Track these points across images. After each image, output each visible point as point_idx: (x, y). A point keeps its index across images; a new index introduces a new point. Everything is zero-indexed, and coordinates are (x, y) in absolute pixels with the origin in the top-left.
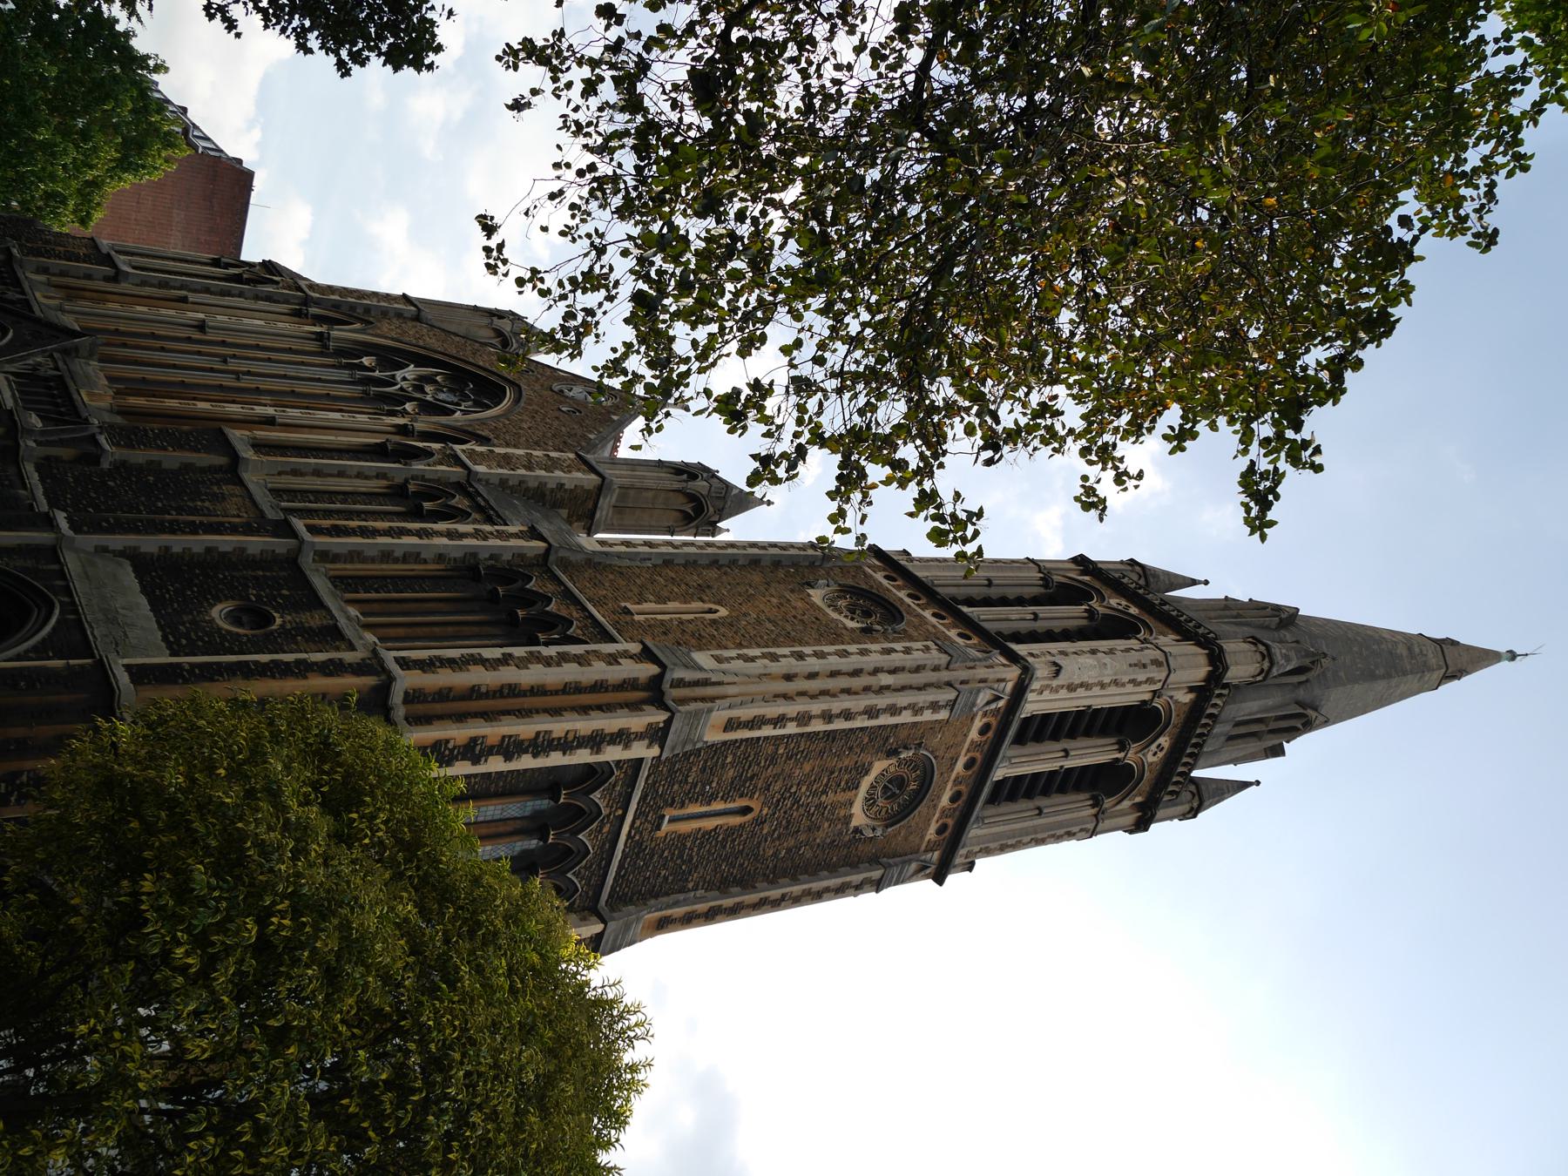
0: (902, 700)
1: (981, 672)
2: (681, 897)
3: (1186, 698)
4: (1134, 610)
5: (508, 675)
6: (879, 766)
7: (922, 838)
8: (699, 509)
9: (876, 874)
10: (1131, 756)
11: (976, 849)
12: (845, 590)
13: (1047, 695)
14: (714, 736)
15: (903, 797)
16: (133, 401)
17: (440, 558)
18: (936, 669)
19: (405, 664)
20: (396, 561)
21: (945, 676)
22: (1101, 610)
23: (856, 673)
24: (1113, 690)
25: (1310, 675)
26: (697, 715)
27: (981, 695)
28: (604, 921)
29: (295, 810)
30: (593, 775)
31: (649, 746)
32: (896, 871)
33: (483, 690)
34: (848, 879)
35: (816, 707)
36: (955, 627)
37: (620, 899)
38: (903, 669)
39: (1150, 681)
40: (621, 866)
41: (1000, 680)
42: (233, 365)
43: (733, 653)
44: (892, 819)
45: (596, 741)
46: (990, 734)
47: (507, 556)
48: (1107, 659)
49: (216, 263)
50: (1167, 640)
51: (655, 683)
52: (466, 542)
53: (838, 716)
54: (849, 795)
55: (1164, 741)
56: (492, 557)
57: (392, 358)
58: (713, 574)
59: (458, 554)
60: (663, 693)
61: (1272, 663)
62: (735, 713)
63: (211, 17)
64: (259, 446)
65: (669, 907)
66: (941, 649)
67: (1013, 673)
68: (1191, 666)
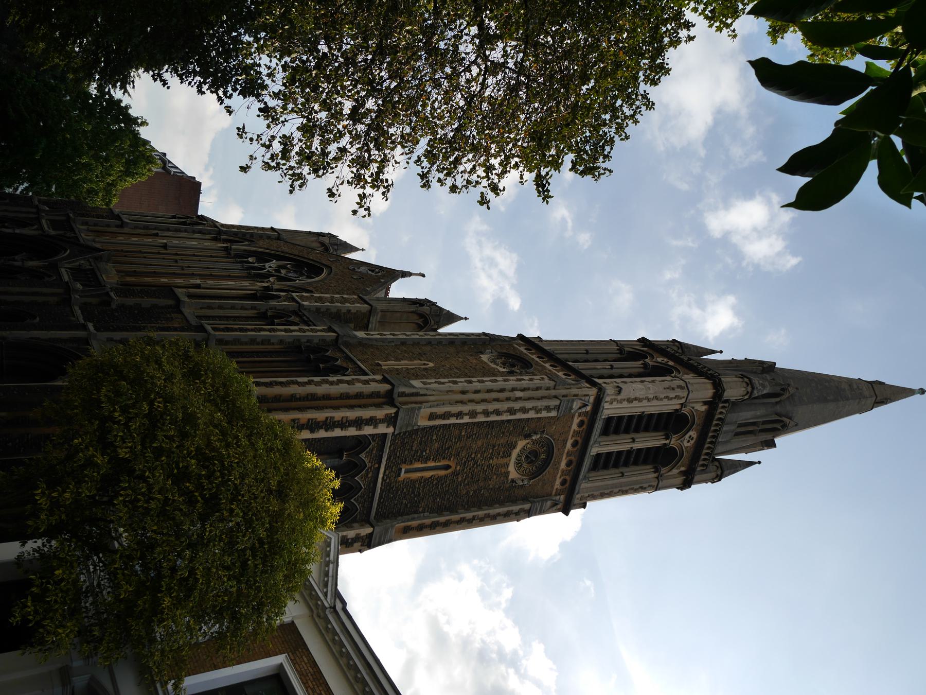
0: (529, 405)
1: (574, 391)
2: (416, 516)
3: (704, 408)
4: (671, 363)
5: (311, 389)
6: (521, 444)
7: (552, 487)
8: (426, 322)
9: (527, 506)
10: (674, 442)
11: (586, 495)
12: (501, 355)
13: (615, 405)
14: (423, 423)
15: (539, 460)
16: (128, 279)
17: (281, 342)
18: (548, 389)
19: (258, 384)
20: (258, 344)
21: (553, 392)
22: (651, 363)
23: (502, 390)
24: (655, 402)
25: (783, 398)
26: (413, 410)
27: (575, 403)
28: (372, 526)
29: (167, 367)
30: (360, 443)
31: (388, 427)
32: (538, 506)
33: (298, 396)
34: (511, 508)
35: (480, 408)
36: (562, 370)
37: (382, 516)
38: (528, 389)
39: (677, 397)
40: (380, 497)
41: (585, 395)
42: (180, 264)
43: (433, 381)
44: (533, 475)
45: (359, 423)
46: (584, 427)
47: (316, 341)
48: (650, 385)
49: (174, 217)
50: (690, 377)
51: (390, 393)
52: (294, 333)
53: (492, 413)
54: (505, 460)
55: (693, 433)
56: (308, 341)
57: (263, 257)
58: (428, 348)
59: (291, 340)
60: (393, 399)
61: (753, 388)
62: (434, 410)
63: (155, 80)
64: (190, 296)
65: (409, 521)
66: (550, 379)
67: (593, 392)
68: (703, 390)
